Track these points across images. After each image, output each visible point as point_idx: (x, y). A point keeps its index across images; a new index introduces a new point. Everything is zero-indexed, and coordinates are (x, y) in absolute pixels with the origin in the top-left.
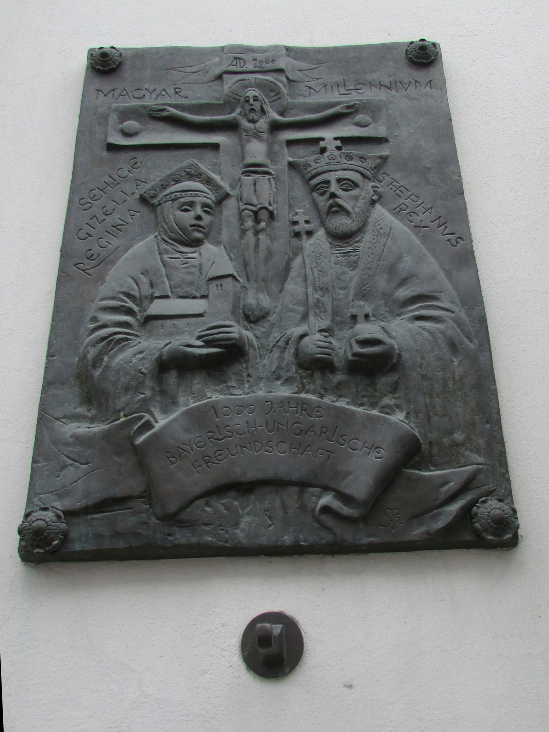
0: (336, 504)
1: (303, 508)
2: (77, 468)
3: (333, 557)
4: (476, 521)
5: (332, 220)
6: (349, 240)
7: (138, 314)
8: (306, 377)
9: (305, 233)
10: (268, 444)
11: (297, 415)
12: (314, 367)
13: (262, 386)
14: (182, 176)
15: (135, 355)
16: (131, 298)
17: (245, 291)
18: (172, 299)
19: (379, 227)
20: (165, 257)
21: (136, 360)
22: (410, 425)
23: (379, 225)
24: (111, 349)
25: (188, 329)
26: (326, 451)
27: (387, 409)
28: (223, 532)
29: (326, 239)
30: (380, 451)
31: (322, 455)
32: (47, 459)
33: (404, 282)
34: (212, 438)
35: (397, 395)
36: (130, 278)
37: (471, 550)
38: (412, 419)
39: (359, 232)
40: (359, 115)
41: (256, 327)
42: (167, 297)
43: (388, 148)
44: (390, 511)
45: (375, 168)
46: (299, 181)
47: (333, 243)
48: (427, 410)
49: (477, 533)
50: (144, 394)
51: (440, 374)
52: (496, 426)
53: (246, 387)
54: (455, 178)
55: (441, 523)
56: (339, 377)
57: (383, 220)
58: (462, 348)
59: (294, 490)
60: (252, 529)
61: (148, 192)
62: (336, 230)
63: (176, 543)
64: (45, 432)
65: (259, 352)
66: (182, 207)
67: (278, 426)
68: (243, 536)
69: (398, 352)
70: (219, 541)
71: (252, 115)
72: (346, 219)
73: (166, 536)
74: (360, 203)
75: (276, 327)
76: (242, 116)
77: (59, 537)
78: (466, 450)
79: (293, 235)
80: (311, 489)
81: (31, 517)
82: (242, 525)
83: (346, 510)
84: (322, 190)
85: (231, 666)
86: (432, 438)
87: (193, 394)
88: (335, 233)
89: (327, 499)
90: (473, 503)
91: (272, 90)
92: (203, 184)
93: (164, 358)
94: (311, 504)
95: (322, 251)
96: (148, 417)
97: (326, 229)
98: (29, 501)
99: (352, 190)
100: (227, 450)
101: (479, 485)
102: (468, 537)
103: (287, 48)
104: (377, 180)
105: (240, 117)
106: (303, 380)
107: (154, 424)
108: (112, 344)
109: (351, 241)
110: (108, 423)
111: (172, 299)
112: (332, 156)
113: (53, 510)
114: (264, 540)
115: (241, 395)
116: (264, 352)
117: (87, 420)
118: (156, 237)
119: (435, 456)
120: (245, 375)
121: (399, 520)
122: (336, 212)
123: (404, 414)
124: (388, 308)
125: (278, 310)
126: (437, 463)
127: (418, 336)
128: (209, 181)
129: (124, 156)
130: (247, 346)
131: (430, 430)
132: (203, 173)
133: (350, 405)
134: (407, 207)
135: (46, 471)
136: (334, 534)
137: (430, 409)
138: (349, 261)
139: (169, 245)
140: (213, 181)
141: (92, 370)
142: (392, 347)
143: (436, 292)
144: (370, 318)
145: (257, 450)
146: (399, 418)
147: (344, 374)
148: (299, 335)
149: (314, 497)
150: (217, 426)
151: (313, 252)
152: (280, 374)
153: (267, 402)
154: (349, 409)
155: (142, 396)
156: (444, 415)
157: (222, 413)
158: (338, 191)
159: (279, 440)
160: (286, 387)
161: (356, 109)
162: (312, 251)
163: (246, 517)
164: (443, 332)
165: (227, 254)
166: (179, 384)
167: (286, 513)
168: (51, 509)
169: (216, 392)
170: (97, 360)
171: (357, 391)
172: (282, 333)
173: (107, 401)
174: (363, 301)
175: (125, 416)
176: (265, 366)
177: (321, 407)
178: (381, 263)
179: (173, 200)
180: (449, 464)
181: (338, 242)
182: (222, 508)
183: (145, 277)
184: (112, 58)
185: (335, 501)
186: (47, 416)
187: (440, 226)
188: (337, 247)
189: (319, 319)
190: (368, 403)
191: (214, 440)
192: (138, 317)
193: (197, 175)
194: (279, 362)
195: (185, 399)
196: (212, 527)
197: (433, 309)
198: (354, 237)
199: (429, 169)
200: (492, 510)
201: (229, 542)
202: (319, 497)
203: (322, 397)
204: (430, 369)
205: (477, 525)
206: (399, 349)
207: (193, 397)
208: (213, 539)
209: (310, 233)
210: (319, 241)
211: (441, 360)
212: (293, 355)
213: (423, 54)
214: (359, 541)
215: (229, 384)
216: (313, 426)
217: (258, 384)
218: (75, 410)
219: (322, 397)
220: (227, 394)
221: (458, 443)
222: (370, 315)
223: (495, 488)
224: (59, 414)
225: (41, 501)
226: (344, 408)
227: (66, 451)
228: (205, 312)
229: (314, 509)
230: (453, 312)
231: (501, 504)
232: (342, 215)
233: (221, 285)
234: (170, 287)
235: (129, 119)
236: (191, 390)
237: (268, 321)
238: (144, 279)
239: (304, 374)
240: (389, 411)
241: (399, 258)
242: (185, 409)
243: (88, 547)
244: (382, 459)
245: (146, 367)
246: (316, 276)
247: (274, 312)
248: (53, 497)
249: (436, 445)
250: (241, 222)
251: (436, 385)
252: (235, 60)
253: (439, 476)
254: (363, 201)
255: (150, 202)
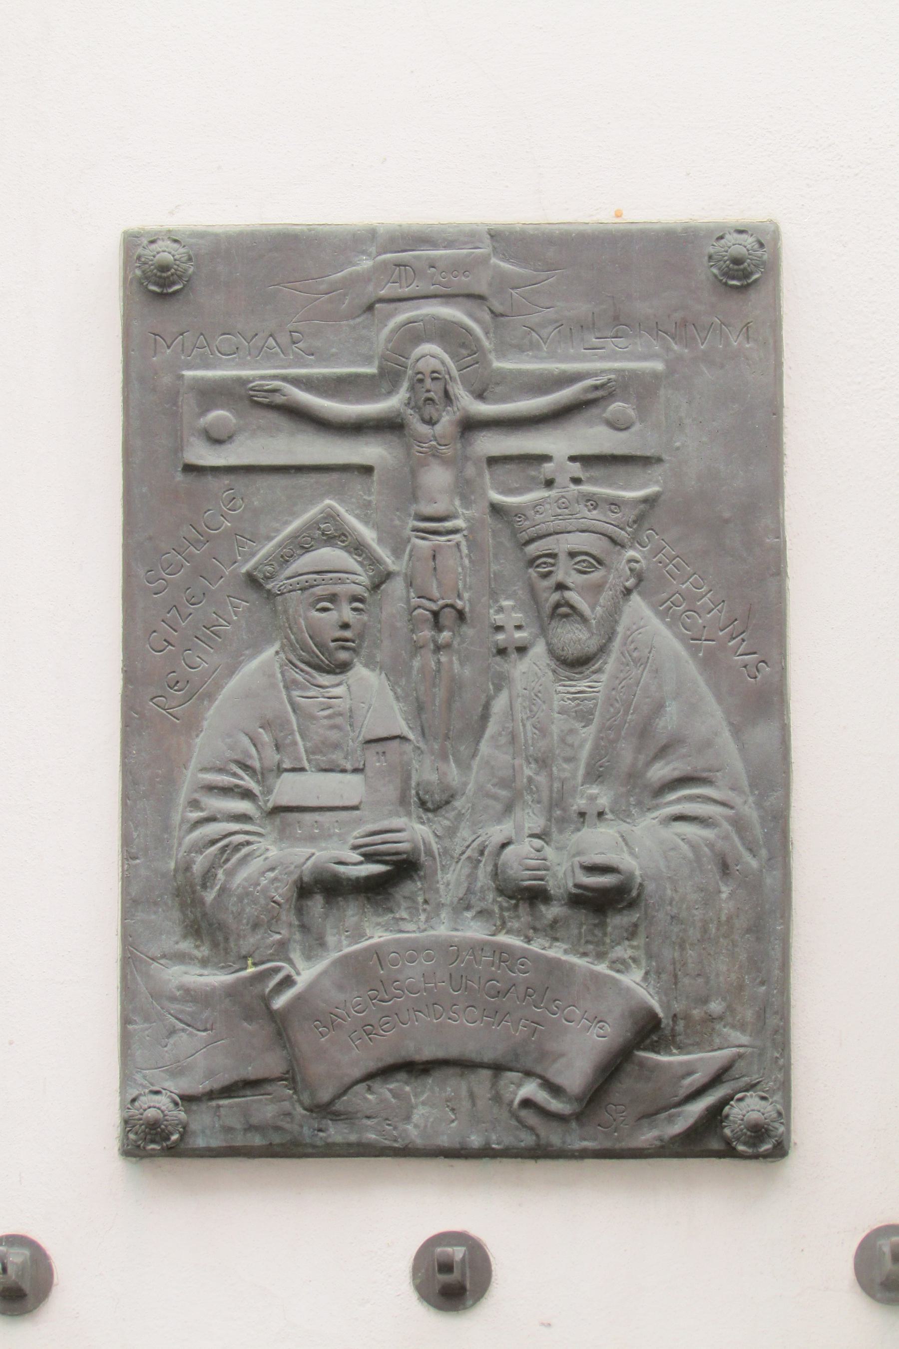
0: (542, 1096)
1: (497, 1098)
2: (191, 1034)
3: (536, 1162)
4: (727, 1126)
5: (559, 630)
6: (584, 669)
7: (260, 798)
8: (508, 909)
9: (515, 650)
10: (451, 1008)
11: (493, 969)
12: (519, 897)
13: (444, 918)
14: (314, 539)
15: (264, 873)
16: (248, 771)
17: (419, 755)
18: (309, 772)
19: (632, 647)
20: (295, 693)
21: (266, 881)
22: (649, 990)
23: (632, 642)
24: (227, 860)
25: (337, 831)
26: (532, 1022)
27: (619, 965)
28: (391, 1128)
29: (548, 665)
30: (603, 1026)
31: (526, 1027)
32: (147, 1019)
33: (663, 752)
34: (374, 999)
35: (635, 943)
36: (244, 735)
37: (722, 1160)
38: (652, 982)
39: (600, 653)
40: (615, 401)
41: (436, 819)
42: (302, 770)
43: (660, 475)
44: (614, 1107)
45: (635, 522)
46: (506, 541)
47: (557, 672)
48: (675, 969)
49: (728, 1143)
50: (279, 933)
51: (698, 914)
52: (775, 989)
53: (422, 920)
54: (770, 540)
55: (679, 1127)
56: (552, 911)
57: (640, 630)
58: (738, 870)
59: (486, 1074)
60: (429, 1124)
61: (259, 568)
62: (563, 650)
63: (330, 1140)
64: (139, 979)
65: (441, 862)
66: (317, 604)
67: (466, 983)
68: (416, 1133)
69: (639, 880)
70: (386, 1139)
71: (429, 410)
72: (580, 630)
73: (316, 1132)
74: (605, 598)
75: (465, 821)
76: (412, 409)
77: (178, 1130)
78: (725, 1026)
79: (494, 651)
80: (510, 1074)
81: (139, 1102)
82: (415, 1118)
83: (555, 1105)
84: (545, 568)
85: (398, 1295)
86: (678, 1010)
87: (347, 931)
88: (562, 656)
89: (530, 1089)
90: (725, 1101)
91: (463, 345)
92: (350, 552)
93: (306, 879)
94: (508, 1095)
95: (540, 688)
96: (287, 969)
97: (548, 644)
98: (126, 1079)
99: (593, 571)
100: (395, 1016)
101: (737, 1076)
102: (715, 1145)
103: (492, 233)
104: (638, 542)
105: (410, 411)
106: (504, 913)
107: (296, 977)
108: (228, 852)
109: (588, 669)
110: (230, 972)
111: (309, 772)
112: (564, 500)
113: (166, 1094)
114: (444, 1141)
115: (414, 931)
116: (448, 860)
117: (196, 961)
118: (277, 653)
119: (680, 1035)
120: (420, 900)
121: (624, 1120)
122: (566, 616)
123: (642, 973)
124: (635, 797)
125: (470, 790)
126: (681, 1045)
127: (672, 853)
128: (358, 548)
129: (213, 483)
130: (423, 854)
131: (676, 998)
132: (350, 534)
133: (568, 954)
134: (684, 599)
135: (148, 1036)
136: (537, 1136)
137: (678, 966)
138: (582, 710)
139: (300, 672)
140: (365, 549)
141: (202, 891)
142: (631, 876)
143: (710, 771)
144: (606, 814)
145: (438, 1016)
146: (634, 979)
147: (562, 905)
148: (500, 844)
149: (512, 1085)
150: (382, 981)
151: (525, 689)
152: (470, 901)
153: (452, 946)
154: (565, 962)
155: (278, 937)
156: (699, 975)
157: (389, 961)
158: (570, 575)
159: (467, 1004)
160: (479, 924)
161: (610, 390)
162: (524, 687)
163: (420, 1107)
164: (711, 846)
165: (391, 690)
166: (326, 916)
167: (474, 1104)
168: (164, 1091)
169: (379, 927)
170: (208, 877)
171: (580, 933)
172: (474, 833)
173: (227, 940)
174: (597, 785)
175: (255, 964)
176: (448, 884)
177: (526, 958)
178: (630, 717)
179: (302, 589)
180: (699, 1046)
181: (566, 671)
182: (388, 1095)
183: (266, 732)
184: (176, 270)
185: (540, 1091)
186: (139, 954)
187: (734, 638)
188: (564, 680)
189: (531, 814)
190: (594, 953)
191: (378, 1002)
192: (260, 803)
193: (339, 537)
194: (470, 884)
195: (335, 938)
196: (375, 1120)
197: (702, 802)
198: (593, 662)
199: (727, 521)
200: (748, 1112)
201: (398, 1142)
202: (519, 1085)
203: (529, 940)
204: (684, 906)
205: (727, 1132)
206: (641, 877)
207: (347, 937)
208: (377, 1137)
209: (522, 650)
210: (536, 668)
211: (702, 891)
212: (489, 875)
213: (737, 270)
214: (570, 1145)
215: (397, 916)
216: (514, 985)
217: (438, 915)
218: (177, 946)
219: (529, 940)
220: (395, 931)
221: (714, 1017)
222: (607, 810)
223: (761, 1079)
224: (155, 951)
225: (146, 1080)
226: (560, 959)
227: (172, 1009)
228: (361, 803)
229: (512, 1102)
230: (732, 808)
231: (763, 1103)
232: (575, 622)
233: (384, 753)
234: (306, 751)
235: (216, 407)
236: (343, 925)
237: (454, 809)
238: (265, 737)
239: (505, 904)
240: (621, 967)
241: (659, 708)
242: (337, 955)
243: (215, 1143)
244: (606, 1038)
245: (282, 892)
246: (529, 734)
247: (463, 794)
248: (163, 1075)
249: (682, 1019)
250: (411, 626)
251: (691, 932)
252: (398, 268)
253: (681, 1064)
254: (611, 592)
255: (264, 587)
